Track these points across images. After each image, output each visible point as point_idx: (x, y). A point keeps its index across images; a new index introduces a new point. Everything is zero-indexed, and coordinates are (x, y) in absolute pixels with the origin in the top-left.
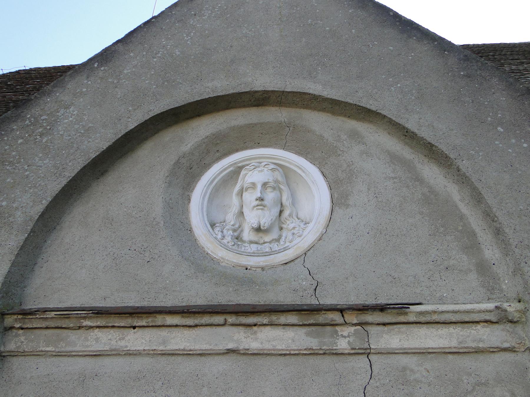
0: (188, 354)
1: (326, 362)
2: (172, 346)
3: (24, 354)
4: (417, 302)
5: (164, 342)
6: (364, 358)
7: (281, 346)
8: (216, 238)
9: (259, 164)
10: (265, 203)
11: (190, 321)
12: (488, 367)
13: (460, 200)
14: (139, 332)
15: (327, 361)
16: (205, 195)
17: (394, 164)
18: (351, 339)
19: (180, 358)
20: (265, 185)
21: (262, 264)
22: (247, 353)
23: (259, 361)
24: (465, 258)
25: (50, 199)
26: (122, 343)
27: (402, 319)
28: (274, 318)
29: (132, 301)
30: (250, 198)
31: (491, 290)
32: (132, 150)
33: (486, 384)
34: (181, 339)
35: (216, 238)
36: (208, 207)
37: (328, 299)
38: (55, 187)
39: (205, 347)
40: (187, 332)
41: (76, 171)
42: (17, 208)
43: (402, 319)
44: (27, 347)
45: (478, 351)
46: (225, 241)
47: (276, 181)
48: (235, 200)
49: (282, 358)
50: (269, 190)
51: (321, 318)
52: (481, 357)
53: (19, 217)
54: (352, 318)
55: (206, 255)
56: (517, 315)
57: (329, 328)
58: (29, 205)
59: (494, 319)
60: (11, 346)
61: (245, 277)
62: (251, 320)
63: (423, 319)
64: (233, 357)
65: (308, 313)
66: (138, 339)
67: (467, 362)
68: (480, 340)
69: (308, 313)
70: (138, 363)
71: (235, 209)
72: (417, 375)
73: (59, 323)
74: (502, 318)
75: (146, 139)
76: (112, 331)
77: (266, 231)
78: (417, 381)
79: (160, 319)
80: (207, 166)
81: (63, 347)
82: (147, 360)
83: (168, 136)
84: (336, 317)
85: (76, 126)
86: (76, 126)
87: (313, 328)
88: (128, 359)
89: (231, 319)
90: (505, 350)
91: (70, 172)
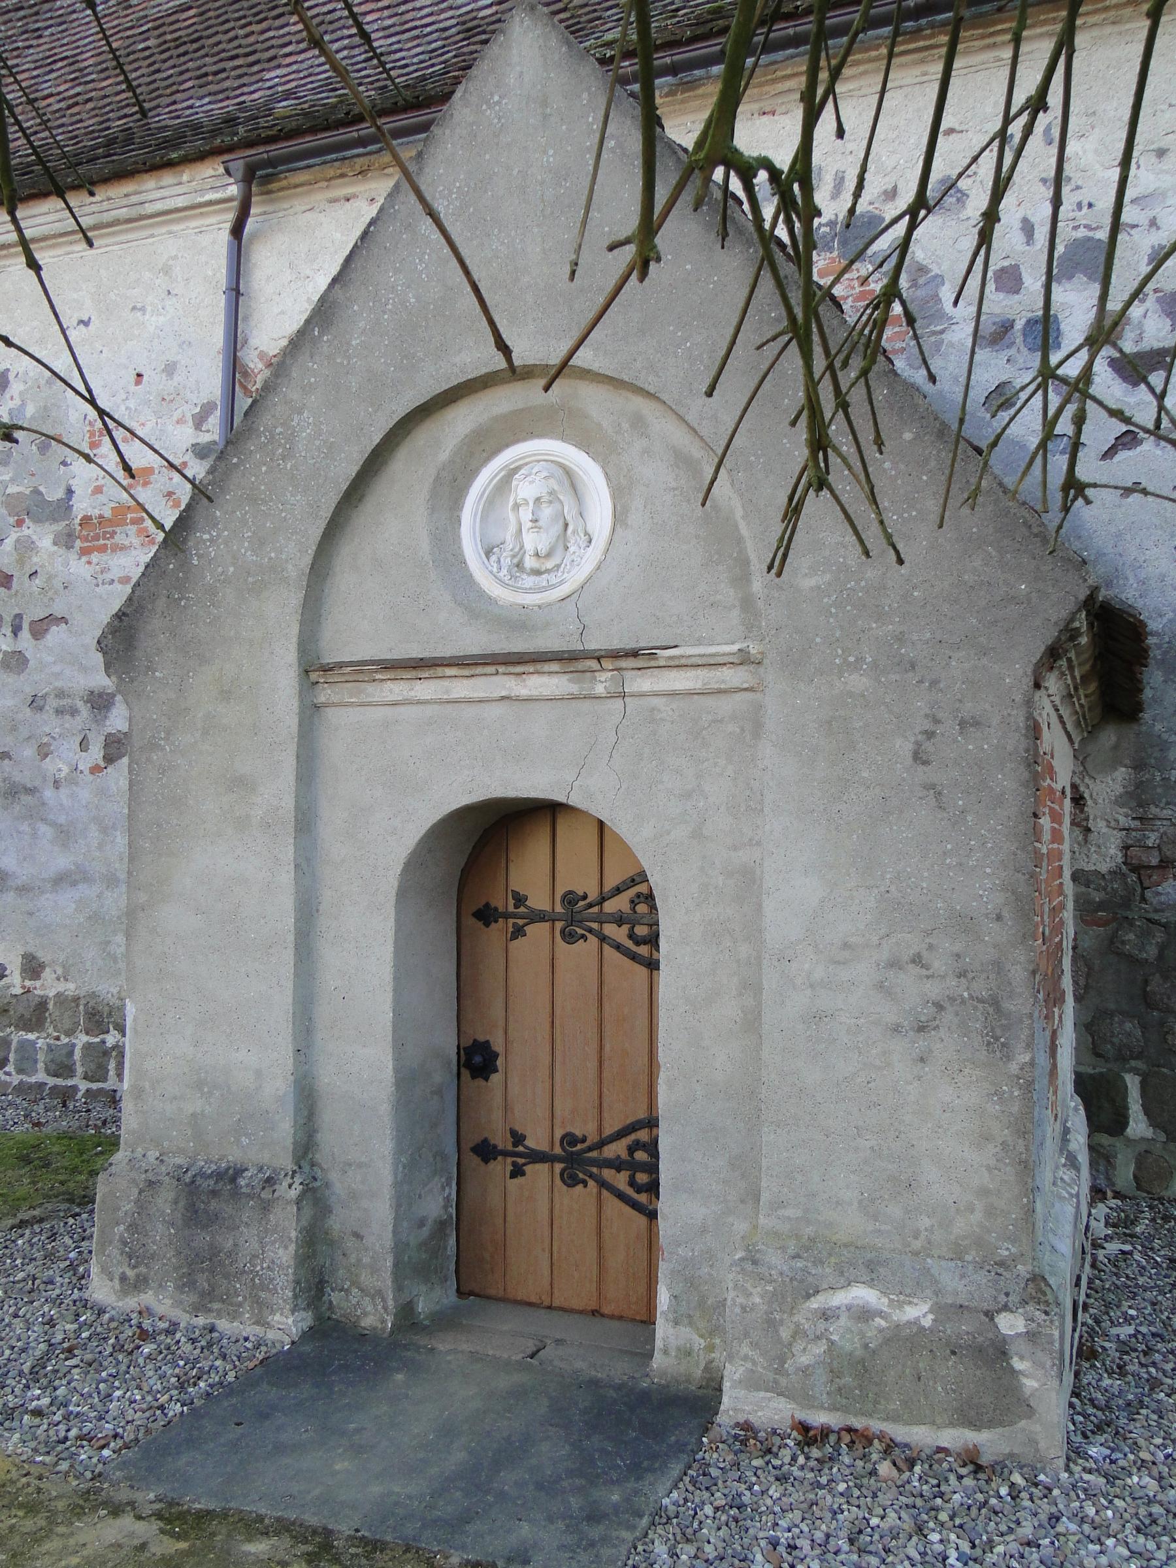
0: (470, 701)
1: (586, 705)
2: (454, 695)
3: (334, 705)
4: (673, 644)
5: (447, 692)
6: (620, 701)
7: (546, 692)
8: (491, 572)
9: (536, 461)
10: (540, 524)
11: (466, 672)
12: (725, 706)
13: (743, 517)
14: (425, 683)
15: (588, 703)
16: (475, 515)
17: (678, 467)
18: (607, 684)
19: (463, 705)
20: (538, 500)
21: (538, 602)
22: (518, 699)
23: (531, 705)
24: (732, 592)
25: (314, 548)
26: (412, 693)
27: (653, 663)
28: (539, 666)
29: (415, 651)
30: (526, 515)
31: (749, 627)
32: (385, 463)
33: (721, 721)
34: (462, 687)
35: (491, 572)
36: (481, 529)
37: (594, 643)
38: (316, 531)
39: (482, 695)
40: (465, 681)
41: (289, 985)
42: (287, 561)
43: (653, 663)
44: (335, 699)
45: (720, 692)
46: (501, 574)
47: (552, 493)
48: (512, 516)
49: (549, 703)
50: (544, 505)
51: (581, 665)
52: (723, 697)
53: (292, 572)
54: (607, 664)
55: (482, 594)
56: (759, 656)
57: (588, 674)
58: (297, 555)
59: (736, 661)
60: (322, 699)
61: (519, 620)
62: (519, 669)
63: (672, 663)
64: (507, 702)
65: (568, 659)
66: (425, 689)
67: (710, 701)
68: (723, 681)
69: (568, 659)
70: (430, 710)
71: (512, 528)
72: (664, 715)
73: (356, 677)
74: (744, 659)
75: (398, 444)
76: (402, 682)
77: (549, 555)
78: (662, 720)
79: (440, 671)
80: (475, 473)
81: (363, 698)
82: (436, 707)
83: (422, 436)
84: (593, 664)
85: (317, 443)
86: (317, 443)
87: (575, 675)
88: (422, 707)
89: (501, 669)
90: (746, 689)
91: (326, 513)
